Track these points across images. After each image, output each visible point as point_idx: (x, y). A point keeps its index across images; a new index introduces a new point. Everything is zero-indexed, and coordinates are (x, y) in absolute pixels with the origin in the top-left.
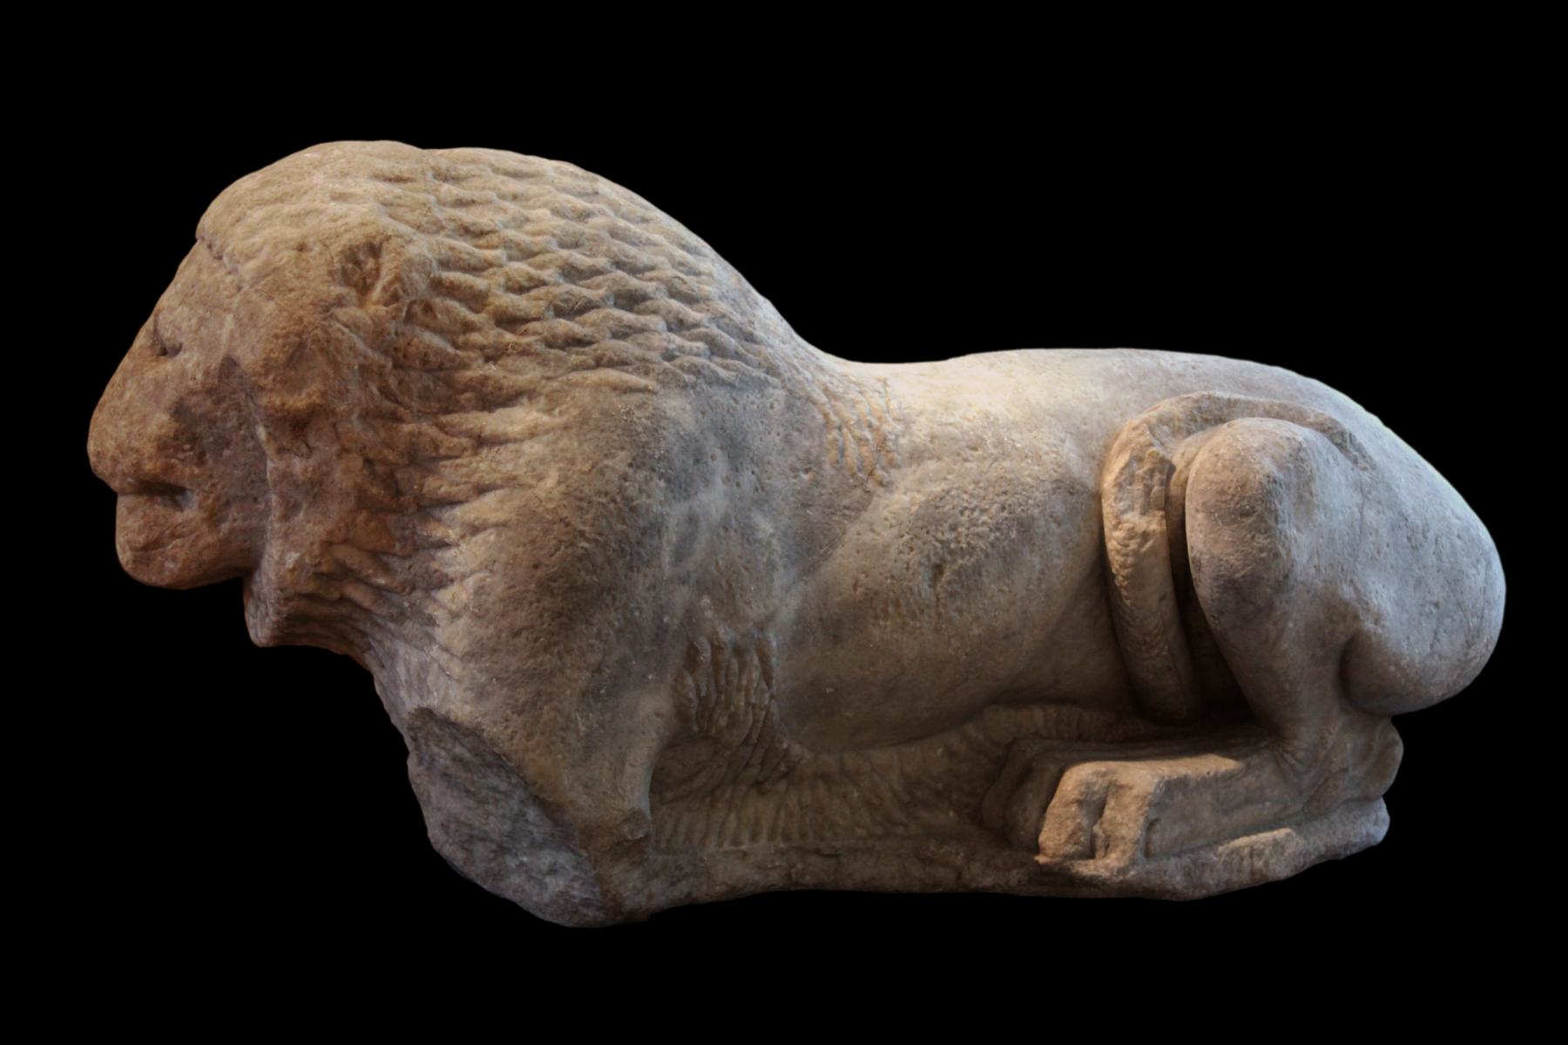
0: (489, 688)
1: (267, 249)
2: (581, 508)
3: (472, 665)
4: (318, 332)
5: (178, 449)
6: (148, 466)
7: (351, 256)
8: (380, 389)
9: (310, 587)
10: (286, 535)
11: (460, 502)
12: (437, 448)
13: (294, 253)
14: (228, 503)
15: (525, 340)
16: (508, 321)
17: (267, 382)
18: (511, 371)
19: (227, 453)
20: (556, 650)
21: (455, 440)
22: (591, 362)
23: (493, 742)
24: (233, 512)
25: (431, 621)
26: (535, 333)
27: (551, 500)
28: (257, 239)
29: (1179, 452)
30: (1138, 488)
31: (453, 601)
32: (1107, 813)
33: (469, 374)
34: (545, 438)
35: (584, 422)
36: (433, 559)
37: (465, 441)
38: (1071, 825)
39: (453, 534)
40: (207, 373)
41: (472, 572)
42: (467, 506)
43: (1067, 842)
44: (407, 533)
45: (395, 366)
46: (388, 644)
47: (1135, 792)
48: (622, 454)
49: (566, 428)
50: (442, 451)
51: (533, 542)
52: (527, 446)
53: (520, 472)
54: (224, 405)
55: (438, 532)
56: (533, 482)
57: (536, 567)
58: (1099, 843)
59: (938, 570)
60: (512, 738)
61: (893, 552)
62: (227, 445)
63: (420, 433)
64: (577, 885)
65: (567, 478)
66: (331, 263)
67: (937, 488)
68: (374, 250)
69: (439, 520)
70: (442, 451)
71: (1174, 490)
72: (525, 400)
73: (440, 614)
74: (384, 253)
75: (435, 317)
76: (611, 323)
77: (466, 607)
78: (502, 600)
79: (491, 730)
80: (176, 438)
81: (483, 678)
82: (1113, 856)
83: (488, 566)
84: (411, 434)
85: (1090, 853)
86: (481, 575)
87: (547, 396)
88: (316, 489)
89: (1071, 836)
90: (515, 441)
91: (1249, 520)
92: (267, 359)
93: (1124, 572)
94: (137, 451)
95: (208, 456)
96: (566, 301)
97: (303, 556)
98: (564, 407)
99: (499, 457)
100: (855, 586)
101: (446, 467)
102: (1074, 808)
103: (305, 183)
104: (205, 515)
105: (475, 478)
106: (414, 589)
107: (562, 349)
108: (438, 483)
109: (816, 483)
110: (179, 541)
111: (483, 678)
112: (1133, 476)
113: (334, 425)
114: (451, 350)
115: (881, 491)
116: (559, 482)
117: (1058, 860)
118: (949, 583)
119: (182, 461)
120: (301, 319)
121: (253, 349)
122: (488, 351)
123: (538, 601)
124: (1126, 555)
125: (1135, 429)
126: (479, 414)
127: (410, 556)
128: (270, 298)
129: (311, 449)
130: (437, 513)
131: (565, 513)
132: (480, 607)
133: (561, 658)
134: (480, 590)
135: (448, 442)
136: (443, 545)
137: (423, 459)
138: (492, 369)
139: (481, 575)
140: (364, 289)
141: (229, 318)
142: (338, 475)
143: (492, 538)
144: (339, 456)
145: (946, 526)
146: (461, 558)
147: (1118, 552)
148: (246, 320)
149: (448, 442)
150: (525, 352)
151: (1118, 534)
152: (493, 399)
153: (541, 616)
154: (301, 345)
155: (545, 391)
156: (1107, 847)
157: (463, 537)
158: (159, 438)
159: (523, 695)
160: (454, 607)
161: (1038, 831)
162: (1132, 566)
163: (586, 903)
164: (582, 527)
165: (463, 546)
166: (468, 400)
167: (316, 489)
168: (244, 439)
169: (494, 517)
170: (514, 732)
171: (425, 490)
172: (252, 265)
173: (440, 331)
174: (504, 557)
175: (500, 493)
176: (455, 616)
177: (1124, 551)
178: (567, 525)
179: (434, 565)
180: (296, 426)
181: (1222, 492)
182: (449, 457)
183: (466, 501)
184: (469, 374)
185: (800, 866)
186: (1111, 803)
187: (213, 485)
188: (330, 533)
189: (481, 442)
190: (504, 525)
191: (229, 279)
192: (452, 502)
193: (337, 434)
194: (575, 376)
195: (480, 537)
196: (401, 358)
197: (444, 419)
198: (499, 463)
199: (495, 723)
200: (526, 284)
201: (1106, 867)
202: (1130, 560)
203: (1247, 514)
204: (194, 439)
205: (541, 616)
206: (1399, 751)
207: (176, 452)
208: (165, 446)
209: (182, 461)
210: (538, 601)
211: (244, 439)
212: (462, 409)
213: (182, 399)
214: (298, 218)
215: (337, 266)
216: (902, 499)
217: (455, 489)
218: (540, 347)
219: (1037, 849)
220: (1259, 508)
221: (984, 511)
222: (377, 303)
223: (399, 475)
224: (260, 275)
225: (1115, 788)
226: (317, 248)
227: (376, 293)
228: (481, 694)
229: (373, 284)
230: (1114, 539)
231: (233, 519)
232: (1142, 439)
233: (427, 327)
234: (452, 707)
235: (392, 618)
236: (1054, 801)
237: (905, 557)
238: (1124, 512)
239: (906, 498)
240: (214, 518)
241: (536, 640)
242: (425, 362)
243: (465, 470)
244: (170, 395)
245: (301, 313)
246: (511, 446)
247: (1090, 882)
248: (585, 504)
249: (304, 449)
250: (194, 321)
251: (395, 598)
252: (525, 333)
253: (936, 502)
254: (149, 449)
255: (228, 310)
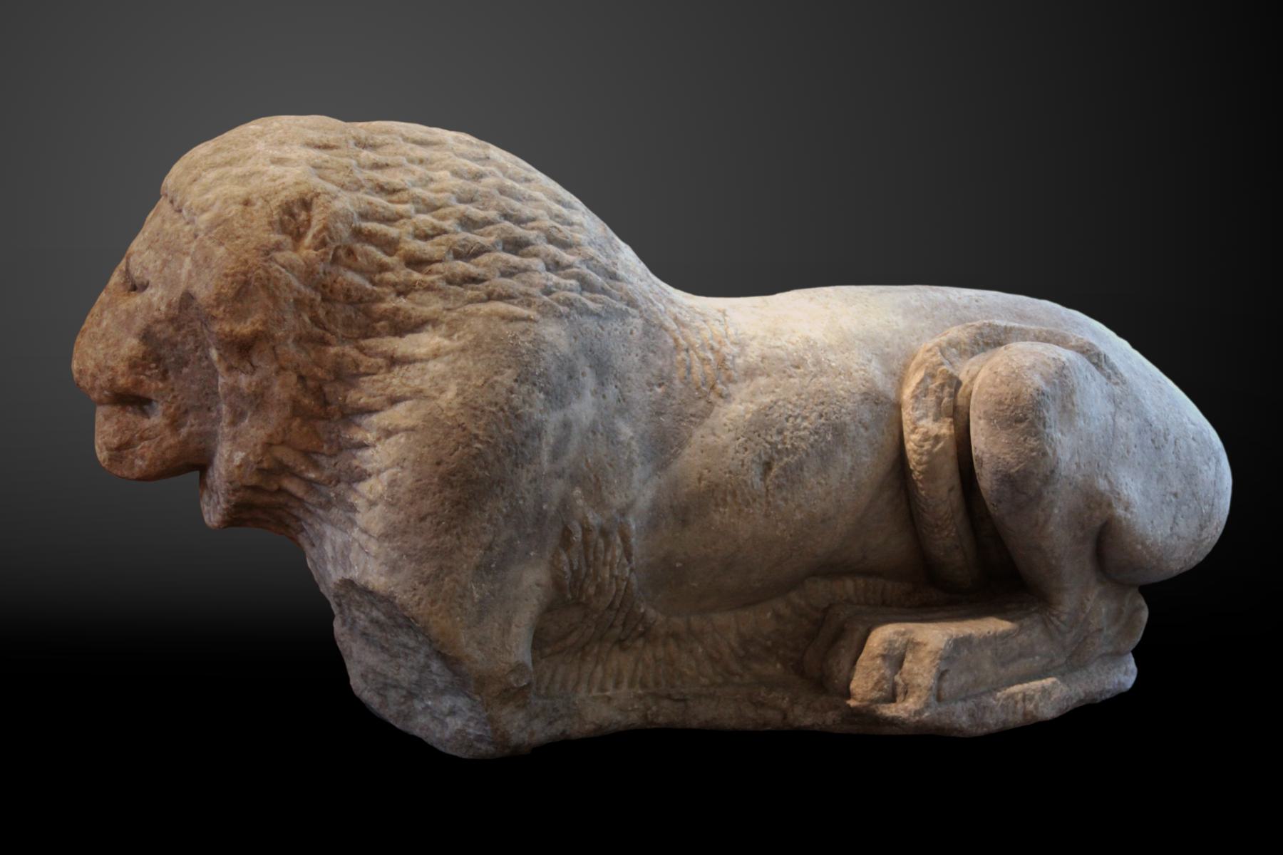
0: (400, 563)
1: (218, 204)
2: (475, 416)
3: (386, 544)
4: (260, 271)
5: (146, 367)
6: (121, 381)
7: (287, 209)
8: (311, 318)
9: (254, 481)
10: (234, 438)
11: (377, 411)
12: (357, 366)
13: (240, 207)
14: (186, 412)
15: (429, 278)
16: (416, 262)
17: (219, 312)
18: (418, 304)
19: (185, 370)
20: (455, 532)
21: (373, 360)
22: (484, 296)
23: (404, 607)
24: (191, 419)
25: (353, 508)
26: (438, 273)
27: (451, 409)
28: (210, 196)
29: (964, 370)
30: (931, 400)
31: (370, 491)
32: (906, 665)
33: (384, 306)
34: (446, 358)
35: (478, 345)
36: (354, 457)
37: (380, 361)
38: (876, 675)
39: (371, 437)
40: (169, 305)
41: (387, 468)
42: (382, 414)
43: (873, 689)
44: (333, 436)
45: (323, 300)
46: (317, 527)
47: (929, 648)
48: (509, 372)
49: (463, 350)
50: (362, 369)
51: (436, 443)
52: (431, 365)
53: (426, 386)
54: (183, 332)
55: (359, 436)
56: (436, 394)
57: (438, 464)
58: (899, 690)
59: (767, 466)
60: (419, 604)
61: (731, 452)
62: (186, 364)
63: (344, 355)
64: (472, 724)
65: (464, 391)
66: (271, 215)
67: (767, 400)
68: (306, 205)
69: (359, 426)
70: (362, 369)
71: (961, 401)
72: (429, 327)
73: (360, 502)
74: (314, 207)
75: (356, 259)
76: (500, 264)
77: (381, 496)
78: (411, 491)
79: (402, 597)
80: (144, 358)
81: (395, 555)
82: (911, 700)
83: (399, 463)
84: (337, 355)
85: (892, 698)
86: (394, 470)
87: (448, 324)
88: (258, 400)
89: (876, 684)
90: (422, 360)
91: (1022, 426)
92: (219, 294)
93: (920, 468)
94: (112, 369)
95: (170, 373)
96: (463, 246)
97: (248, 455)
98: (461, 333)
99: (408, 374)
100: (700, 480)
101: (365, 382)
102: (879, 661)
103: (250, 150)
104: (167, 421)
105: (389, 391)
106: (338, 482)
107: (460, 285)
108: (358, 395)
109: (668, 395)
110: (146, 443)
111: (395, 555)
112: (927, 389)
113: (274, 348)
114: (369, 286)
115: (720, 401)
116: (458, 395)
117: (865, 703)
118: (777, 477)
119: (149, 377)
120: (246, 261)
121: (207, 286)
122: (400, 287)
123: (440, 492)
124: (921, 454)
125: (929, 351)
126: (392, 339)
127: (335, 455)
128: (221, 244)
129: (254, 368)
130: (357, 420)
131: (462, 420)
132: (393, 496)
133: (459, 538)
134: (393, 483)
135: (367, 362)
136: (362, 446)
137: (346, 375)
138: (402, 302)
139: (394, 470)
140: (298, 236)
141: (188, 260)
142: (276, 389)
143: (403, 440)
144: (277, 373)
145: (774, 430)
146: (377, 457)
147: (915, 452)
148: (201, 262)
149: (367, 362)
150: (429, 288)
151: (915, 437)
152: (403, 326)
153: (443, 504)
154: (246, 283)
155: (446, 320)
156: (906, 693)
157: (379, 439)
158: (130, 359)
159: (428, 569)
160: (371, 497)
161: (849, 680)
162: (926, 463)
163: (479, 739)
164: (476, 431)
165: (379, 447)
166: (383, 327)
167: (258, 400)
168: (200, 359)
169: (404, 423)
170: (421, 599)
171: (348, 401)
172: (206, 217)
173: (360, 271)
174: (412, 456)
175: (409, 403)
176: (372, 504)
177: (920, 451)
178: (464, 429)
179: (355, 463)
180: (242, 349)
181: (1000, 403)
182: (367, 374)
183: (382, 410)
184: (384, 306)
185: (654, 708)
186: (909, 657)
187: (175, 397)
188: (270, 436)
189: (394, 361)
190: (412, 429)
191: (187, 228)
192: (370, 411)
193: (276, 355)
194: (471, 308)
195: (393, 439)
196: (328, 293)
197: (363, 343)
198: (408, 378)
199: (405, 592)
200: (430, 232)
201: (905, 709)
202: (925, 458)
203: (1020, 421)
204: (159, 359)
205: (443, 504)
206: (1145, 615)
207: (144, 370)
208: (135, 365)
209: (149, 377)
210: (440, 492)
211: (200, 359)
212: (378, 335)
213: (149, 326)
214: (244, 178)
215: (276, 217)
216: (738, 408)
217: (372, 400)
218: (442, 284)
219: (849, 695)
220: (1030, 416)
221: (805, 418)
222: (309, 248)
223: (326, 389)
224: (213, 225)
225: (912, 645)
226: (260, 203)
227: (308, 240)
228: (394, 568)
229: (305, 233)
230: (912, 441)
231: (191, 425)
232: (934, 359)
233: (349, 268)
234: (370, 578)
235: (321, 506)
236: (863, 655)
237: (740, 456)
238: (920, 419)
239: (742, 408)
240: (175, 423)
241: (439, 523)
242: (348, 296)
243: (380, 385)
244: (139, 323)
245: (247, 256)
246: (418, 365)
247: (892, 722)
248: (478, 413)
249: (249, 367)
250: (159, 263)
251: (323, 489)
252: (430, 273)
253: (766, 411)
254: (122, 367)
255: (187, 254)
